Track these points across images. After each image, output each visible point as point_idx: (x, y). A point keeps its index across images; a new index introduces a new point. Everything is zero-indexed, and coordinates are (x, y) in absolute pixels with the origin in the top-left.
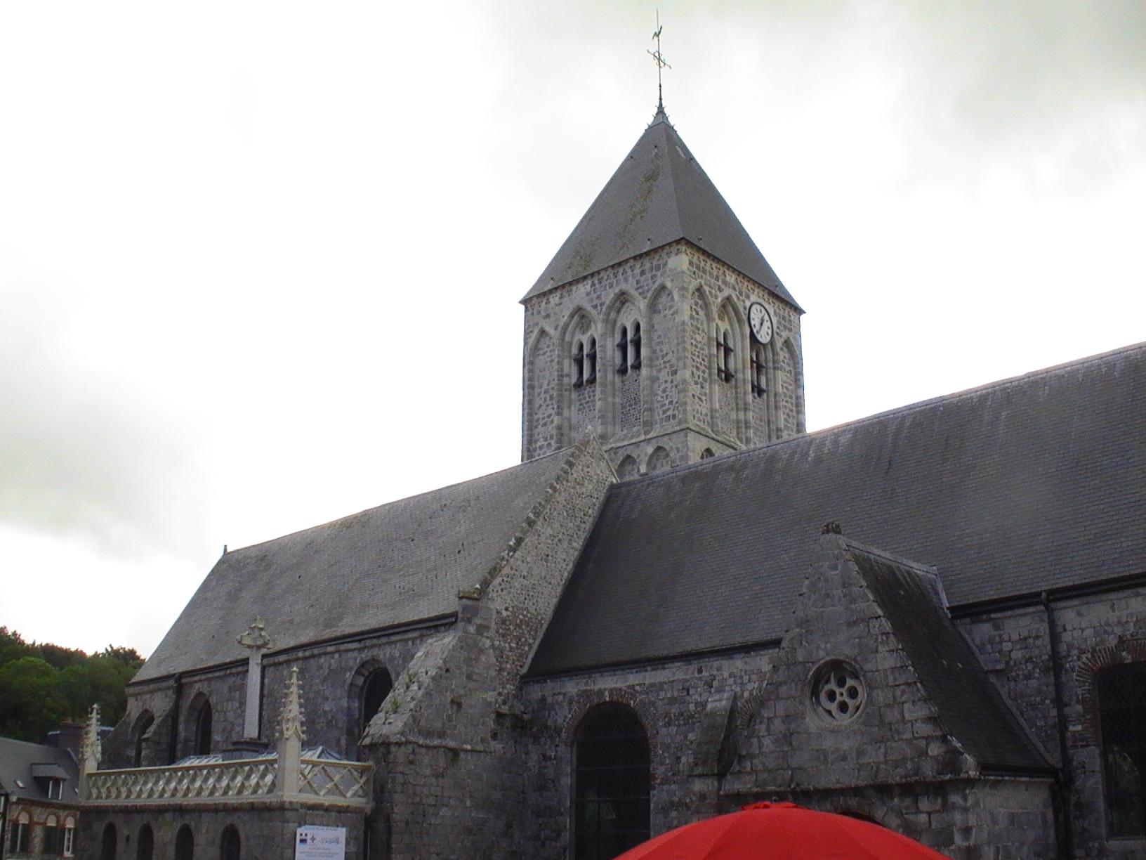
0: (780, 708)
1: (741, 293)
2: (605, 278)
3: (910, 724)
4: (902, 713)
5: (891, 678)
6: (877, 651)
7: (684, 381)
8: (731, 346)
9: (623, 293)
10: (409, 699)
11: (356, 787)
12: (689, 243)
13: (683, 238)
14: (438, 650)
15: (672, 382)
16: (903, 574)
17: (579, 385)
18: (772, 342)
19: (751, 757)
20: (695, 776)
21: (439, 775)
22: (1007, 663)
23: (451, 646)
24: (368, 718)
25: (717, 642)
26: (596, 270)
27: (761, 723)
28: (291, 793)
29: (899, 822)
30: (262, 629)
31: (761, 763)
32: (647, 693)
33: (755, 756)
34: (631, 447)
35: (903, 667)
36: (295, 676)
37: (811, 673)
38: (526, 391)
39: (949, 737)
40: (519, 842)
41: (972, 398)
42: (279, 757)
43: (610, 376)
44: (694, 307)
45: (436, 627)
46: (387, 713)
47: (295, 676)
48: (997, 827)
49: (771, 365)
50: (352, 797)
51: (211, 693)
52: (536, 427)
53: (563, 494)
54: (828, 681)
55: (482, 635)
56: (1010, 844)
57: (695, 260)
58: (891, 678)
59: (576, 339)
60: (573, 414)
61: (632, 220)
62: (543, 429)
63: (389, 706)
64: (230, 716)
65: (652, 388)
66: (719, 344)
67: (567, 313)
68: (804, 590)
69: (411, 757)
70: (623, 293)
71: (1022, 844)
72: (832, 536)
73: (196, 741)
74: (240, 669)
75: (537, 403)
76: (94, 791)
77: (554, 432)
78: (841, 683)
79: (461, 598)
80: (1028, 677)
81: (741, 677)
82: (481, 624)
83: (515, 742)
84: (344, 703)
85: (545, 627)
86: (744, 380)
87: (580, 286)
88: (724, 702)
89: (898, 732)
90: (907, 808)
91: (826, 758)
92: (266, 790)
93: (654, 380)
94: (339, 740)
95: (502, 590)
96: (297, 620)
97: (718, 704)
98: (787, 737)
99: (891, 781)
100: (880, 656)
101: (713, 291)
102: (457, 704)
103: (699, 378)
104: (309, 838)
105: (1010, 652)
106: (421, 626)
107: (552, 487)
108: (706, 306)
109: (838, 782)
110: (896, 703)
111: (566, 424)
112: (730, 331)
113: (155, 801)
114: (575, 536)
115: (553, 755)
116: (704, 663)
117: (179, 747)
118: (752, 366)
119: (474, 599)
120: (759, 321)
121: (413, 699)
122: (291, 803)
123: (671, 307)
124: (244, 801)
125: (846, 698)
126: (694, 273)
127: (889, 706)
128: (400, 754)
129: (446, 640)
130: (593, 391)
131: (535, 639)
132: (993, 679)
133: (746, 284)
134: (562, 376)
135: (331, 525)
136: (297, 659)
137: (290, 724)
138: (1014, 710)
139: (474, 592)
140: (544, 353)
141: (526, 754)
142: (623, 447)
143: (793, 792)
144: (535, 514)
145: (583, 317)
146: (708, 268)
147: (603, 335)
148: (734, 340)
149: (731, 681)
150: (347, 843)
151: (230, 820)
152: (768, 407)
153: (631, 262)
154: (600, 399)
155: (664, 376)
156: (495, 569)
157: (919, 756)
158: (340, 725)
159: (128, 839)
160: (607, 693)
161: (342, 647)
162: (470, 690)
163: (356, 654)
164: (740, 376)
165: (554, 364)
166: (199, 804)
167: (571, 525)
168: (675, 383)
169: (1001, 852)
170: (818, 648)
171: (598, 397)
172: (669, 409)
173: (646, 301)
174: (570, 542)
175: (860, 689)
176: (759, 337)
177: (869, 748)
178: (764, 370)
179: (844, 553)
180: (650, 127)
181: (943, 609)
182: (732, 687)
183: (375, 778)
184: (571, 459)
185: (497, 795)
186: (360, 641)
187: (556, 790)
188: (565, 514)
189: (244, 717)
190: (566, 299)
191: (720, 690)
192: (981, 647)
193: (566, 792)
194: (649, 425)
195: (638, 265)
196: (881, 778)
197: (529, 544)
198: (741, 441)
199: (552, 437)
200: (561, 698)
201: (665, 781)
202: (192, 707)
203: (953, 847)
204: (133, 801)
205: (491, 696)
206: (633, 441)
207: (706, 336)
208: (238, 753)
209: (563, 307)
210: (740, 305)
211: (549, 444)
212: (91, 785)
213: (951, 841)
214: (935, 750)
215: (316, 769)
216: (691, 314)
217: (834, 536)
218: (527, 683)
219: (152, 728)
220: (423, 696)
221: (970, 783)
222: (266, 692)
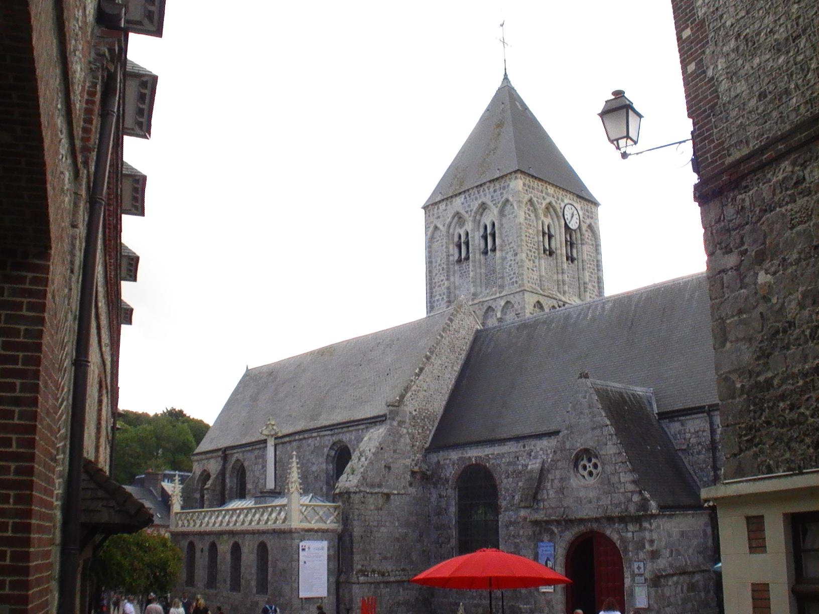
1: (558, 199)
2: (472, 194)
4: (619, 478)
5: (613, 459)
6: (606, 444)
7: (522, 260)
8: (552, 232)
9: (483, 204)
11: (332, 518)
12: (523, 172)
13: (518, 170)
15: (515, 260)
17: (459, 261)
18: (579, 227)
19: (543, 500)
21: (379, 509)
22: (688, 445)
23: (383, 435)
24: (338, 478)
26: (467, 188)
28: (296, 523)
29: (618, 537)
30: (273, 425)
32: (495, 459)
35: (620, 453)
37: (573, 455)
38: (428, 265)
39: (643, 492)
42: (288, 502)
43: (477, 256)
44: (527, 212)
45: (375, 423)
46: (348, 474)
48: (671, 539)
50: (331, 523)
51: (244, 460)
52: (434, 287)
53: (447, 339)
54: (583, 460)
57: (527, 182)
58: (613, 459)
60: (456, 279)
62: (439, 289)
63: (349, 470)
64: (257, 474)
66: (544, 234)
67: (450, 216)
68: (569, 409)
69: (363, 499)
70: (483, 204)
71: (689, 547)
72: (584, 380)
73: (236, 488)
74: (261, 446)
75: (435, 271)
76: (180, 523)
77: (445, 291)
78: (590, 460)
80: (699, 453)
82: (400, 421)
83: (423, 487)
84: (324, 466)
86: (561, 255)
87: (458, 198)
88: (537, 465)
90: (622, 529)
94: (321, 489)
95: (412, 399)
96: (294, 414)
97: (534, 466)
98: (561, 490)
99: (613, 515)
103: (531, 256)
104: (307, 547)
105: (690, 439)
106: (365, 422)
108: (535, 210)
109: (587, 515)
110: (616, 472)
111: (452, 286)
112: (552, 224)
113: (217, 528)
114: (455, 363)
115: (445, 495)
116: (526, 442)
117: (227, 492)
118: (566, 244)
119: (396, 406)
120: (571, 215)
121: (362, 466)
122: (296, 529)
123: (513, 213)
125: (592, 469)
126: (527, 190)
127: (612, 474)
128: (356, 498)
129: (381, 430)
130: (468, 265)
131: (433, 427)
132: (680, 454)
133: (561, 192)
134: (449, 256)
135: (312, 353)
136: (295, 440)
137: (293, 484)
138: (692, 472)
139: (396, 402)
140: (438, 241)
142: (486, 301)
143: (564, 520)
144: (430, 352)
145: (460, 218)
146: (536, 186)
147: (473, 230)
150: (328, 549)
151: (261, 539)
152: (578, 269)
153: (488, 184)
154: (472, 271)
155: (510, 256)
158: (322, 478)
159: (202, 550)
160: (473, 459)
161: (322, 434)
162: (395, 459)
163: (329, 437)
164: (559, 252)
165: (444, 247)
168: (516, 261)
169: (674, 553)
171: (472, 269)
172: (513, 277)
173: (498, 209)
174: (452, 367)
175: (599, 464)
176: (570, 226)
178: (575, 246)
180: (499, 89)
181: (653, 414)
182: (542, 456)
183: (343, 513)
185: (413, 519)
186: (331, 430)
188: (449, 351)
190: (449, 206)
191: (536, 458)
192: (675, 436)
193: (453, 516)
194: (502, 287)
195: (492, 185)
196: (608, 514)
197: (427, 371)
198: (560, 292)
199: (444, 294)
200: (448, 461)
203: (645, 550)
204: (204, 528)
205: (408, 462)
206: (493, 297)
207: (535, 230)
209: (447, 212)
211: (443, 298)
212: (177, 518)
214: (636, 498)
215: (309, 509)
216: (525, 217)
217: (584, 380)
218: (429, 453)
219: (210, 482)
221: (653, 516)
222: (277, 459)
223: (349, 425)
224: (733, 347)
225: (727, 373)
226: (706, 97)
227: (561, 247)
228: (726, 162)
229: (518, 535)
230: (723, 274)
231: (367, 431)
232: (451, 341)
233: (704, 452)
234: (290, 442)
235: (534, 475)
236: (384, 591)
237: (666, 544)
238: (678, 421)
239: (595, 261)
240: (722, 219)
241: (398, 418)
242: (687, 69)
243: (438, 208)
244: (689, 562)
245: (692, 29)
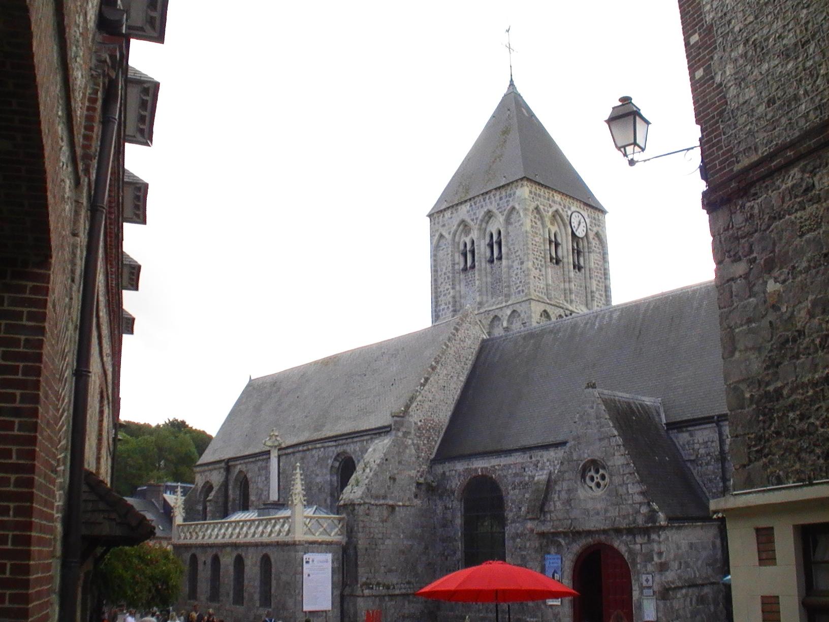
0: (565, 485)
2: (478, 201)
3: (631, 496)
6: (614, 455)
7: (528, 269)
8: (559, 240)
9: (489, 212)
10: (365, 478)
11: (336, 530)
12: (529, 180)
13: (524, 177)
14: (381, 447)
15: (521, 269)
16: (638, 407)
17: (465, 270)
18: (587, 235)
19: (550, 512)
20: (528, 519)
24: (342, 488)
25: (540, 441)
27: (555, 493)
28: (300, 535)
30: (277, 436)
31: (556, 515)
33: (553, 512)
34: (497, 310)
35: (628, 464)
36: (298, 468)
37: (580, 466)
40: (433, 557)
41: (688, 292)
43: (483, 264)
44: (533, 220)
45: (380, 434)
46: (352, 486)
47: (298, 468)
49: (586, 250)
51: (248, 471)
54: (590, 470)
55: (406, 438)
56: (689, 559)
57: (533, 190)
58: (621, 471)
59: (462, 240)
60: (462, 288)
61: (494, 162)
65: (509, 272)
66: (550, 242)
68: (577, 420)
69: (367, 512)
71: (698, 560)
72: (590, 390)
74: (264, 457)
75: (440, 281)
76: (182, 535)
77: (451, 300)
78: (597, 472)
79: (393, 417)
80: (708, 464)
81: (554, 462)
83: (429, 500)
84: (328, 478)
85: (444, 430)
86: (568, 263)
87: (463, 206)
88: (544, 476)
89: (626, 500)
90: (630, 541)
91: (588, 514)
92: (285, 533)
93: (510, 267)
95: (417, 410)
96: (297, 425)
98: (569, 502)
100: (616, 457)
101: (546, 208)
102: (392, 479)
104: (310, 561)
105: (699, 449)
106: (370, 433)
107: (445, 344)
108: (542, 218)
110: (623, 484)
111: (458, 295)
113: (220, 540)
116: (533, 453)
117: (230, 504)
119: (401, 416)
121: (367, 477)
122: (299, 541)
123: (519, 221)
124: (273, 540)
125: (599, 480)
126: (533, 198)
127: (621, 485)
128: (360, 510)
129: (386, 441)
130: (474, 274)
131: (438, 437)
132: (689, 464)
134: (454, 264)
135: (316, 363)
136: (299, 451)
137: (297, 496)
138: (701, 483)
140: (442, 250)
141: (436, 506)
143: (572, 532)
144: (435, 362)
145: (466, 226)
146: (542, 193)
148: (561, 237)
149: (548, 464)
150: (333, 562)
155: (516, 264)
156: (412, 398)
157: (636, 513)
159: (205, 563)
160: (479, 470)
161: (326, 444)
164: (565, 260)
166: (246, 543)
167: (458, 367)
170: (584, 453)
171: (478, 278)
172: (519, 286)
173: (504, 217)
176: (577, 234)
177: (610, 508)
178: (582, 254)
179: (597, 399)
180: (505, 95)
182: (548, 467)
184: (457, 326)
185: (418, 531)
186: (336, 441)
187: (453, 527)
188: (454, 360)
189: (269, 486)
191: (542, 469)
192: (683, 447)
193: (459, 528)
194: (508, 296)
195: (498, 193)
197: (433, 381)
198: (567, 302)
199: (449, 303)
201: (513, 521)
202: (236, 479)
203: (653, 563)
204: (206, 541)
205: (413, 473)
206: (499, 306)
208: (267, 510)
209: (453, 220)
213: (652, 559)
214: (644, 510)
219: (213, 493)
220: (373, 476)
221: (662, 528)
225: (735, 382)
226: (714, 103)
227: (568, 255)
228: (735, 169)
238: (688, 431)
239: (603, 269)
240: (731, 226)
245: (700, 35)
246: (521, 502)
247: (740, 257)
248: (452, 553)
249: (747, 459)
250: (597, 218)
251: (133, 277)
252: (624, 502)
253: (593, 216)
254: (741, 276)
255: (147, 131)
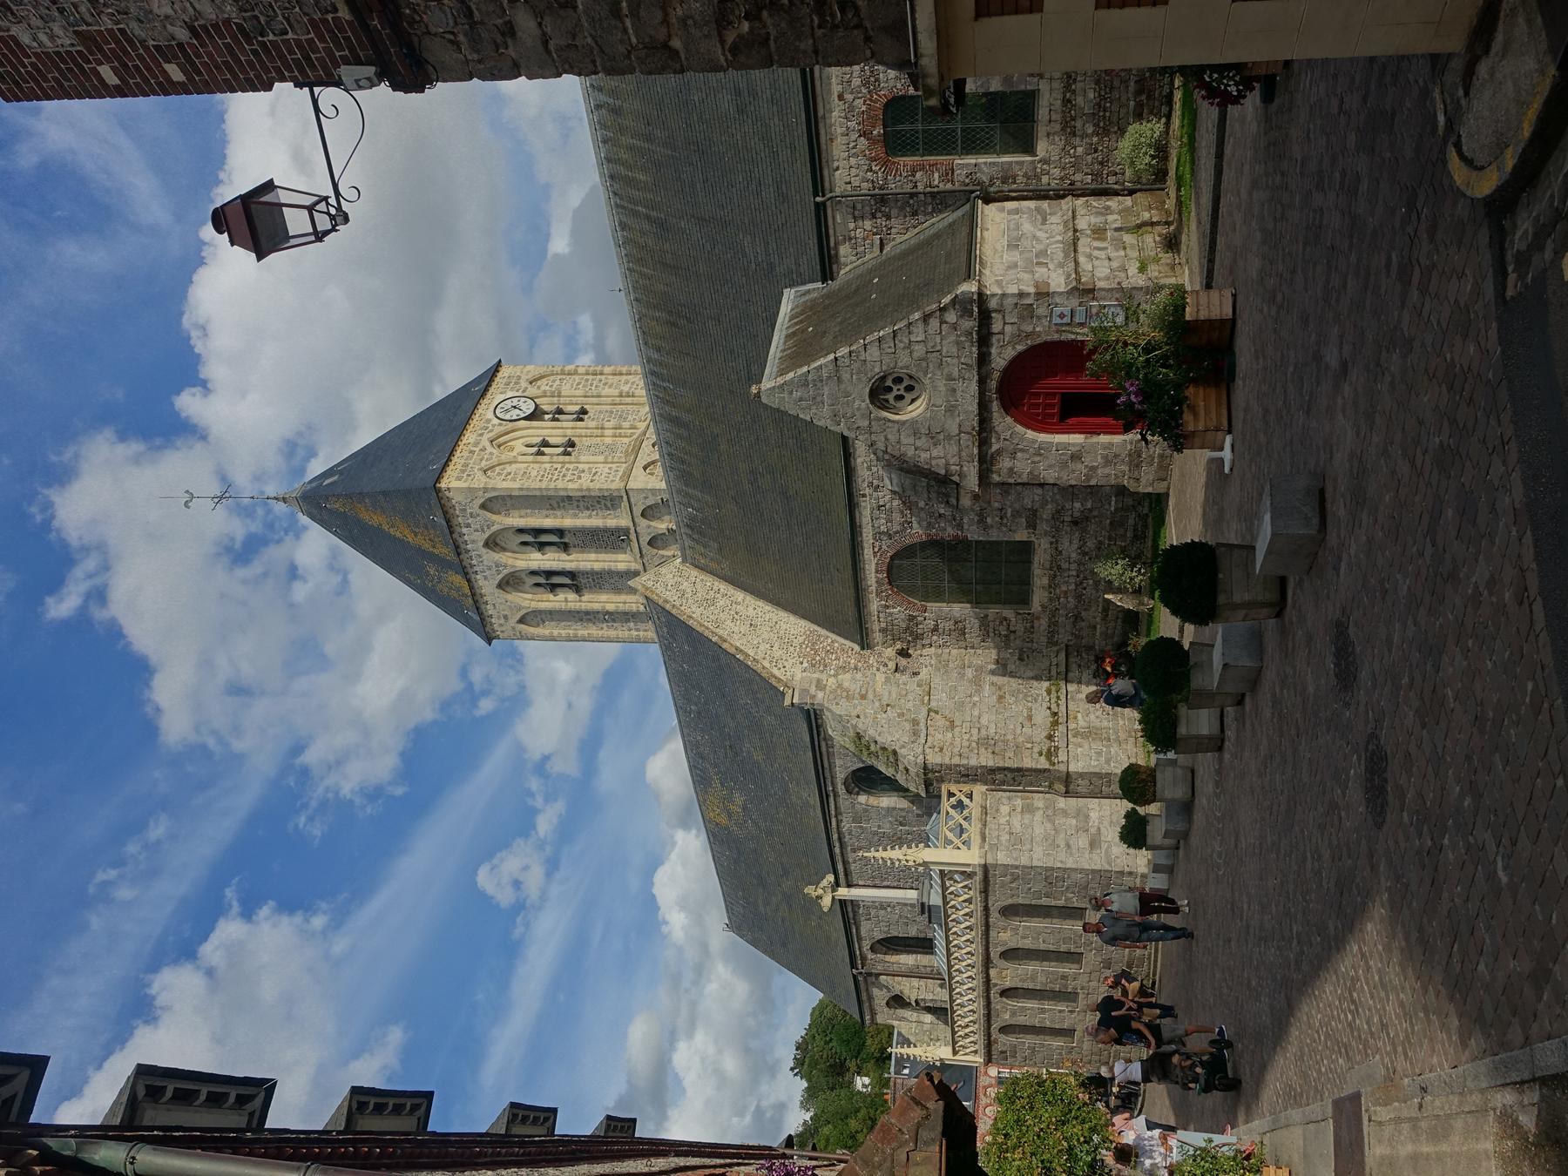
8: (538, 440)
19: (947, 464)
44: (503, 477)
45: (818, 727)
66: (540, 453)
69: (937, 749)
78: (890, 389)
85: (816, 628)
98: (931, 435)
106: (816, 743)
125: (902, 387)
126: (469, 475)
143: (979, 433)
164: (569, 432)
169: (1041, 260)
177: (946, 371)
181: (823, 288)
186: (827, 796)
195: (458, 529)
201: (960, 526)
205: (880, 678)
210: (498, 430)
223: (820, 768)
224: (679, 33)
225: (723, 48)
226: (227, 46)
227: (562, 428)
228: (348, 17)
229: (1001, 510)
230: (552, 47)
231: (832, 739)
232: (696, 605)
233: (887, 210)
234: (845, 863)
235: (908, 482)
236: (1082, 723)
237: (1026, 272)
238: (836, 248)
239: (588, 377)
240: (452, 37)
241: (813, 690)
242: (178, 83)
243: (491, 616)
244: (1060, 238)
245: (101, 64)
246: (931, 515)
247: (506, 23)
248: (1005, 623)
249: (856, 32)
250: (505, 380)
251: (391, 1104)
252: (939, 348)
253: (502, 386)
254: (540, 24)
255: (243, 1091)
